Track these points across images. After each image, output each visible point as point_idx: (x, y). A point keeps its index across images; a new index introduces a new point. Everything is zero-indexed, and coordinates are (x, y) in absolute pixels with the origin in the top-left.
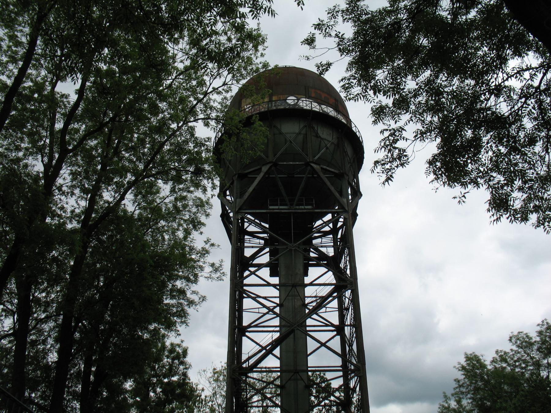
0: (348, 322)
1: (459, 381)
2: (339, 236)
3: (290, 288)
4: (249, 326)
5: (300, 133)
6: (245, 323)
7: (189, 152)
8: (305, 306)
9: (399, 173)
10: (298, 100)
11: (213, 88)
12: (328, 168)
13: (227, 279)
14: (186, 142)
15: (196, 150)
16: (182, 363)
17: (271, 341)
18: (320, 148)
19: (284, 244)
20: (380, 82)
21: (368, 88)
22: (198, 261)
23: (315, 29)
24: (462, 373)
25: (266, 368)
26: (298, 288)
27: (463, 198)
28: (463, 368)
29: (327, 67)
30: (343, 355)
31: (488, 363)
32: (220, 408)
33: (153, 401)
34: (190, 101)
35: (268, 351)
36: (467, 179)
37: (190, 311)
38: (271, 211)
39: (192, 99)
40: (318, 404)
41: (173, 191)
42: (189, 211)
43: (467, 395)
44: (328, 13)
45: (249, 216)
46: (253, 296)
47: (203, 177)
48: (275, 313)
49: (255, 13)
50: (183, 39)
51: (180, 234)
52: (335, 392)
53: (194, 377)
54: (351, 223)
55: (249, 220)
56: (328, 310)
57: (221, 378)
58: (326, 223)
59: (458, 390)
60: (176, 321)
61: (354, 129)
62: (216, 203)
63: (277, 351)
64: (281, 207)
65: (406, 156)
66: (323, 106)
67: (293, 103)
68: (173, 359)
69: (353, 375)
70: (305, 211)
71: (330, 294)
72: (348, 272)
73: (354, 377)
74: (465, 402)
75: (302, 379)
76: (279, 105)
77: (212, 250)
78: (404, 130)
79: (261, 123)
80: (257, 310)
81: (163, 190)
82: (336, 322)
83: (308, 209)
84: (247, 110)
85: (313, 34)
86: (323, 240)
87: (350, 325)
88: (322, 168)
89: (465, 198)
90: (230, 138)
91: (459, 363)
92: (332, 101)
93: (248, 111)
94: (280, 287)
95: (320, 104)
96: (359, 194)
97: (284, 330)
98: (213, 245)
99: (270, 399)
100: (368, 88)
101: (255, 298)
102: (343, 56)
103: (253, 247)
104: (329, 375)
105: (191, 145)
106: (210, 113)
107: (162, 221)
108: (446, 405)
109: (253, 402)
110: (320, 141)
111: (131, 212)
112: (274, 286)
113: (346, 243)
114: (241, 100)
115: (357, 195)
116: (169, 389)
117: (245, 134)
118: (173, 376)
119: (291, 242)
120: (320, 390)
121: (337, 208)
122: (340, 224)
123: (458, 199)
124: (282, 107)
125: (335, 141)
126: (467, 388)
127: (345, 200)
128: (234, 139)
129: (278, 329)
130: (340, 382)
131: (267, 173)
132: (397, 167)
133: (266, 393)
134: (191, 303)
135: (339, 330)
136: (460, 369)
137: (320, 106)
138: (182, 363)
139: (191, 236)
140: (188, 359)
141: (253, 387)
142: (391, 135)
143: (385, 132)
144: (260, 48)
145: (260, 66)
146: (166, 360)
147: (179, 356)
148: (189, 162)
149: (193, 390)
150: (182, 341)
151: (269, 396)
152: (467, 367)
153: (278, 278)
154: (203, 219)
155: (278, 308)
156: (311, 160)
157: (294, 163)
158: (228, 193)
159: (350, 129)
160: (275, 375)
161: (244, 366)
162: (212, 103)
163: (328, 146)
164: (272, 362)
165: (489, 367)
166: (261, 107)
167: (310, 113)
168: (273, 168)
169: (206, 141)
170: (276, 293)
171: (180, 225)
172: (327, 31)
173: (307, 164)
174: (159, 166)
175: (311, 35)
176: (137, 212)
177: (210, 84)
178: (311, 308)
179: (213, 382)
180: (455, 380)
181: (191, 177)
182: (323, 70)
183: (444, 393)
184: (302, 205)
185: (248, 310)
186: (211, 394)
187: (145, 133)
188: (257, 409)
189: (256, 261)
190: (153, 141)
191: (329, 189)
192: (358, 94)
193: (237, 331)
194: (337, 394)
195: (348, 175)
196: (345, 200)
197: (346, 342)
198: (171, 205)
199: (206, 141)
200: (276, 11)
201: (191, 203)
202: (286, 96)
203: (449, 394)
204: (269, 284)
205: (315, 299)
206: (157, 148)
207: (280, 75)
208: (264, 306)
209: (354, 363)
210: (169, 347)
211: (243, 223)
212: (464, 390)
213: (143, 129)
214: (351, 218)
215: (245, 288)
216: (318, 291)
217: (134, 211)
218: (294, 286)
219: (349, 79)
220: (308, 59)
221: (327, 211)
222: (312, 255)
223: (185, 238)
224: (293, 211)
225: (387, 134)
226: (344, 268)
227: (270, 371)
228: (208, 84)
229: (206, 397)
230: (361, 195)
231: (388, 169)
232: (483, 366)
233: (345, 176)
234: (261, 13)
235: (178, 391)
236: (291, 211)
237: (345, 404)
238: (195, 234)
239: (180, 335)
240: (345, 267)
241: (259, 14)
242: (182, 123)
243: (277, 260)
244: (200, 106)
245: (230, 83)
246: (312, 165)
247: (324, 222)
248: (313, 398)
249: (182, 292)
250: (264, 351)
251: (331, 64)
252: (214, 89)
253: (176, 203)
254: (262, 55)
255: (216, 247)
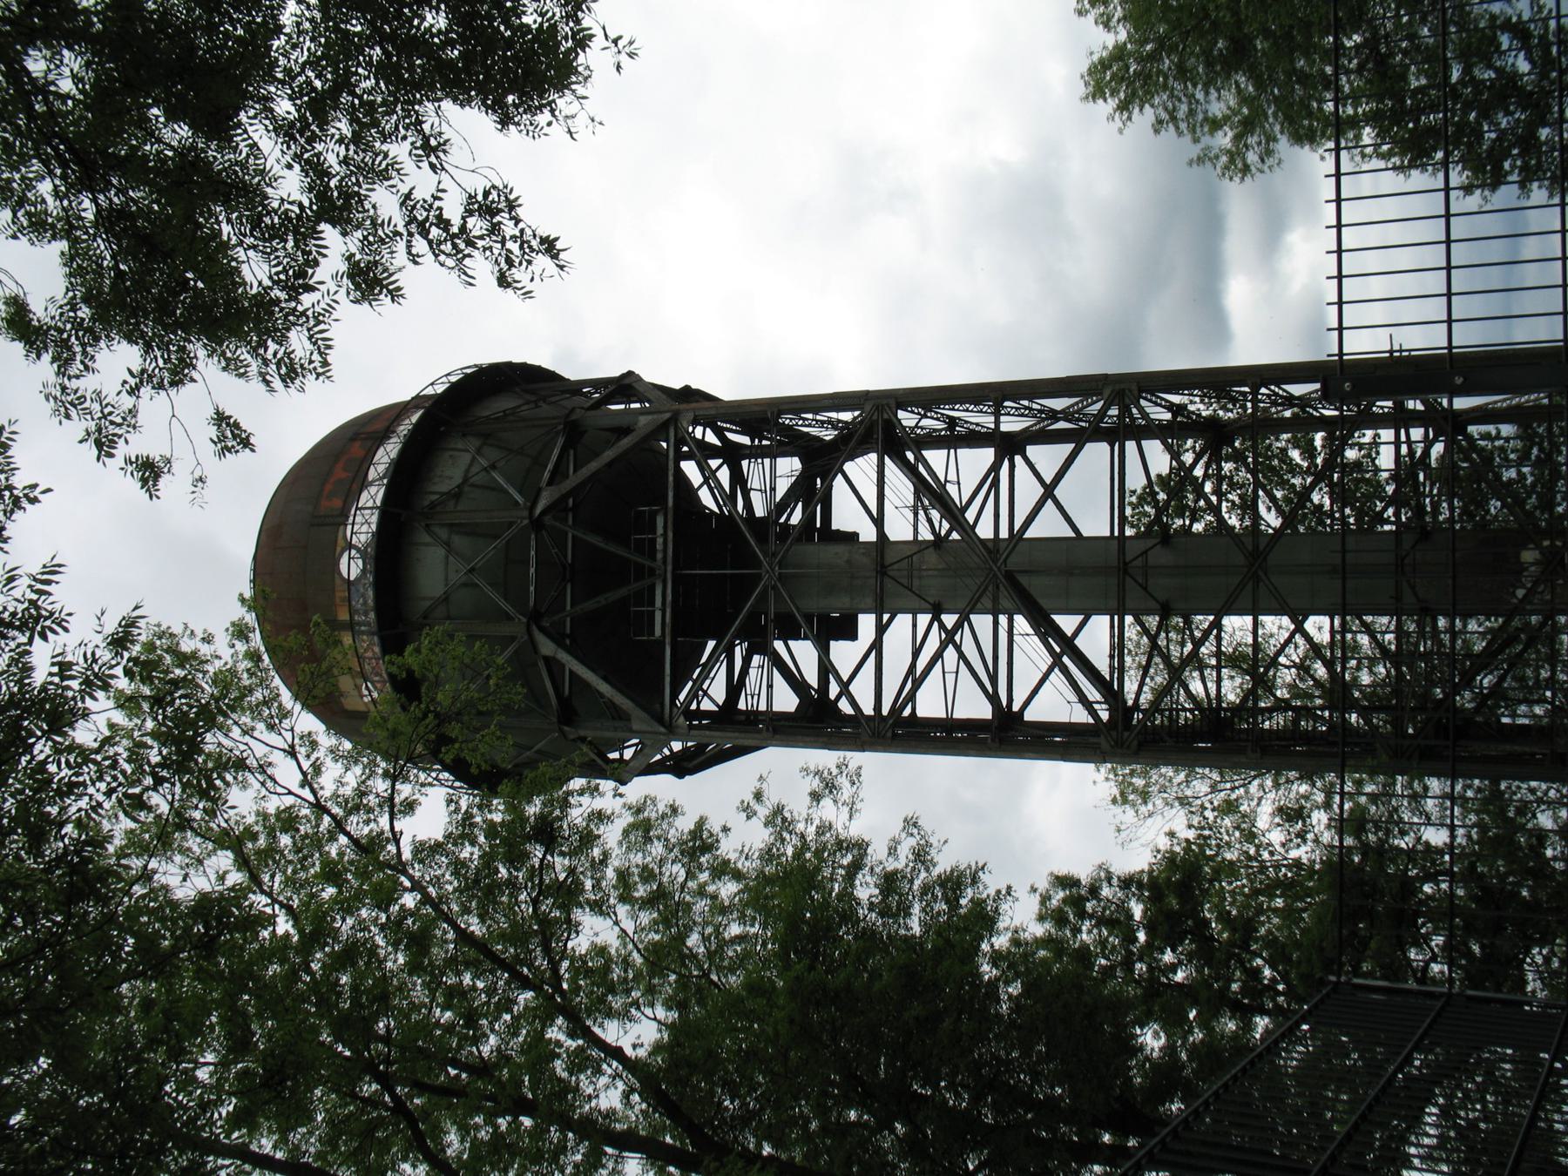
0: (988, 421)
1: (1160, 122)
2: (745, 440)
3: (889, 584)
4: (993, 698)
5: (447, 544)
6: (984, 711)
7: (488, 859)
8: (939, 541)
9: (536, 217)
10: (350, 546)
11: (302, 786)
12: (550, 466)
13: (856, 758)
14: (458, 866)
15: (482, 839)
16: (1094, 891)
17: (1036, 638)
18: (493, 489)
19: (763, 597)
20: (277, 274)
21: (295, 309)
22: (803, 836)
23: (111, 455)
24: (1137, 110)
25: (1112, 657)
26: (889, 559)
27: (621, 43)
28: (1124, 107)
29: (228, 425)
30: (1078, 439)
31: (1110, 40)
32: (1222, 786)
33: (1199, 970)
34: (341, 854)
35: (1065, 649)
36: (565, 29)
37: (944, 863)
38: (668, 630)
39: (333, 851)
40: (1216, 510)
41: (599, 907)
42: (662, 863)
43: (1197, 102)
44: (68, 417)
45: (682, 697)
46: (909, 685)
47: (561, 819)
48: (958, 626)
49: (48, 623)
50: (155, 872)
51: (728, 889)
52: (1181, 464)
53: (1138, 860)
54: (707, 404)
55: (693, 695)
56: (952, 476)
57: (1139, 782)
58: (709, 476)
59: (1183, 126)
60: (972, 900)
61: (440, 389)
62: (639, 787)
63: (1067, 623)
64: (658, 603)
65: (486, 194)
66: (372, 474)
67: (360, 562)
68: (1082, 915)
69: (1134, 411)
70: (670, 535)
71: (911, 470)
72: (847, 416)
73: (1141, 410)
74: (1217, 109)
75: (1146, 552)
76: (365, 603)
77: (773, 797)
78: (410, 193)
79: (410, 648)
80: (950, 678)
81: (597, 934)
82: (987, 455)
83: (665, 527)
84: (375, 695)
85: (128, 461)
86: (756, 485)
87: (997, 414)
88: (550, 483)
89: (620, 37)
90: (452, 741)
91: (1111, 118)
92: (357, 449)
93: (380, 692)
94: (885, 608)
95: (364, 484)
96: (627, 381)
97: (1005, 603)
98: (758, 796)
99: (1198, 644)
100: (295, 309)
101: (914, 678)
102: (195, 374)
103: (770, 686)
104: (1135, 481)
105: (466, 852)
106: (378, 795)
107: (690, 943)
108: (1224, 159)
109: (1207, 694)
110: (473, 485)
111: (660, 1031)
112: (881, 629)
113: (765, 420)
114: (346, 711)
115: (630, 386)
116: (1166, 928)
117: (440, 697)
118: (1130, 917)
119: (759, 577)
120: (1177, 507)
121: (664, 445)
122: (711, 438)
123: (624, 58)
124: (371, 593)
125: (473, 443)
126: (1180, 100)
127: (643, 420)
128: (454, 730)
129: (1003, 619)
130: (1154, 448)
131: (558, 640)
132: (517, 221)
133: (1181, 658)
134: (921, 856)
135: (1009, 447)
136: (1126, 115)
137: (371, 484)
138: (1094, 891)
139: (733, 856)
140: (1084, 873)
141: (1162, 693)
142: (425, 233)
143: (414, 251)
144: (186, 646)
145: (241, 647)
146: (1084, 936)
147: (1072, 898)
148: (516, 858)
149: (1171, 859)
150: (1034, 890)
151: (1189, 647)
152: (1122, 95)
153: (860, 616)
154: (685, 824)
155: (944, 617)
156: (526, 513)
157: (533, 561)
158: (614, 755)
159: (438, 400)
160: (1131, 631)
161: (1105, 716)
162: (347, 791)
163: (484, 463)
164: (1096, 637)
165: (1123, 35)
166: (369, 654)
167: (388, 512)
168: (546, 623)
169: (457, 810)
170: (903, 621)
171: (701, 892)
172: (119, 420)
173: (537, 524)
174: (527, 949)
175: (130, 468)
176: (661, 1012)
177: (290, 793)
178: (946, 525)
179: (1150, 806)
180: (1157, 131)
181: (563, 854)
182: (235, 437)
183: (1190, 163)
184: (653, 541)
185: (950, 704)
186: (1182, 812)
187: (432, 986)
188: (1226, 684)
189: (812, 678)
190: (452, 963)
191: (610, 464)
192: (310, 338)
193: (1006, 733)
194: (1188, 458)
195: (573, 410)
196: (643, 420)
197: (1042, 430)
198: (642, 914)
199: (457, 810)
200: (46, 560)
201: (638, 859)
202: (338, 581)
203: (1195, 151)
204: (877, 646)
205: (921, 512)
206: (477, 953)
207: (268, 589)
208: (938, 655)
209: (1106, 406)
210: (1048, 925)
211: (700, 714)
212: (1183, 109)
213: (419, 993)
214: (694, 405)
215: (885, 712)
216: (899, 504)
217: (659, 1022)
218: (882, 569)
219: (266, 362)
220: (201, 479)
221: (671, 473)
222: (796, 517)
223: (738, 875)
224: (670, 568)
225: (420, 245)
226: (834, 428)
227: (1118, 647)
228: (289, 800)
229: (1190, 826)
230: (630, 373)
231: (521, 247)
232: (1119, 54)
233: (574, 417)
234: (49, 608)
235: (1174, 903)
236: (669, 576)
237: (1215, 436)
238: (728, 848)
239: (1009, 888)
240: (833, 424)
241: (52, 614)
242: (403, 878)
243: (809, 618)
244: (356, 825)
245: (288, 736)
246: (538, 511)
247: (706, 481)
248: (1198, 527)
249: (890, 882)
250: (1065, 659)
251: (218, 413)
252: (305, 783)
253: (637, 900)
254: (208, 639)
255: (765, 786)
